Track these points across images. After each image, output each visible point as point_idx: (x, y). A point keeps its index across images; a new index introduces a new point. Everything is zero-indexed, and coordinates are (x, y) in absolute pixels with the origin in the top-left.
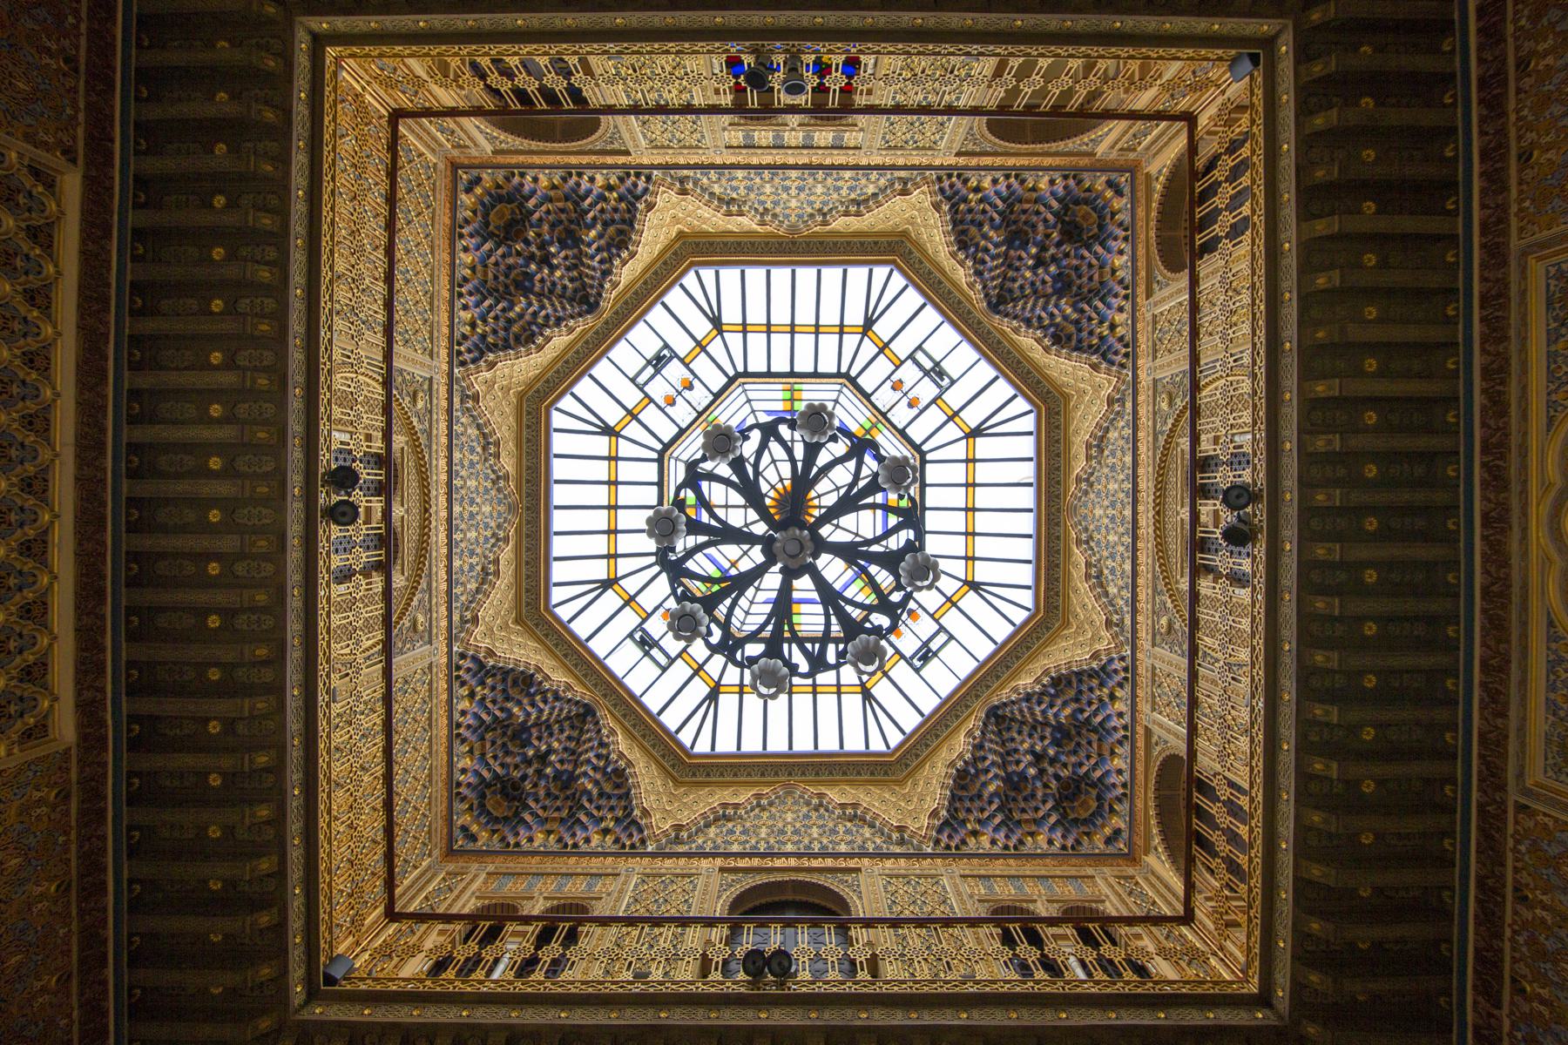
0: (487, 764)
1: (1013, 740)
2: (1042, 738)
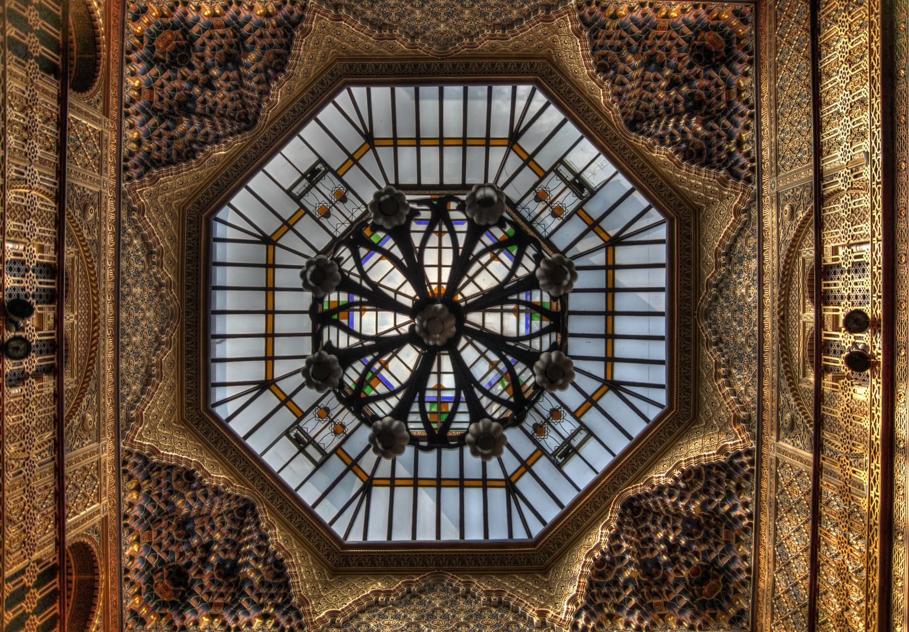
0: (724, 80)
1: (232, 100)
2: (204, 102)
